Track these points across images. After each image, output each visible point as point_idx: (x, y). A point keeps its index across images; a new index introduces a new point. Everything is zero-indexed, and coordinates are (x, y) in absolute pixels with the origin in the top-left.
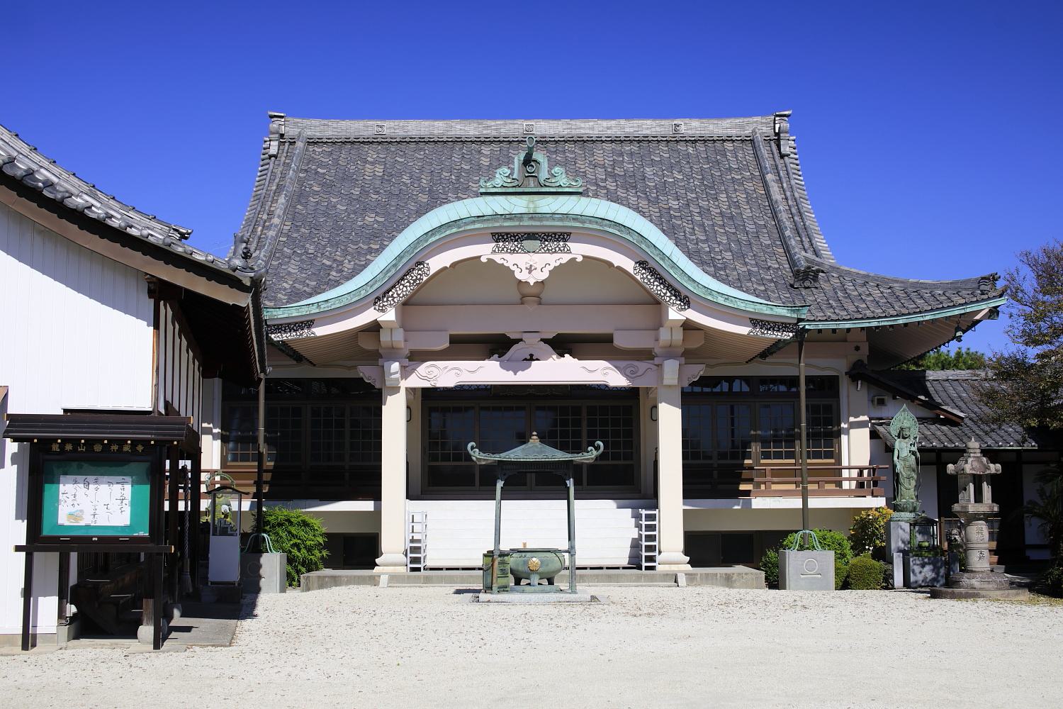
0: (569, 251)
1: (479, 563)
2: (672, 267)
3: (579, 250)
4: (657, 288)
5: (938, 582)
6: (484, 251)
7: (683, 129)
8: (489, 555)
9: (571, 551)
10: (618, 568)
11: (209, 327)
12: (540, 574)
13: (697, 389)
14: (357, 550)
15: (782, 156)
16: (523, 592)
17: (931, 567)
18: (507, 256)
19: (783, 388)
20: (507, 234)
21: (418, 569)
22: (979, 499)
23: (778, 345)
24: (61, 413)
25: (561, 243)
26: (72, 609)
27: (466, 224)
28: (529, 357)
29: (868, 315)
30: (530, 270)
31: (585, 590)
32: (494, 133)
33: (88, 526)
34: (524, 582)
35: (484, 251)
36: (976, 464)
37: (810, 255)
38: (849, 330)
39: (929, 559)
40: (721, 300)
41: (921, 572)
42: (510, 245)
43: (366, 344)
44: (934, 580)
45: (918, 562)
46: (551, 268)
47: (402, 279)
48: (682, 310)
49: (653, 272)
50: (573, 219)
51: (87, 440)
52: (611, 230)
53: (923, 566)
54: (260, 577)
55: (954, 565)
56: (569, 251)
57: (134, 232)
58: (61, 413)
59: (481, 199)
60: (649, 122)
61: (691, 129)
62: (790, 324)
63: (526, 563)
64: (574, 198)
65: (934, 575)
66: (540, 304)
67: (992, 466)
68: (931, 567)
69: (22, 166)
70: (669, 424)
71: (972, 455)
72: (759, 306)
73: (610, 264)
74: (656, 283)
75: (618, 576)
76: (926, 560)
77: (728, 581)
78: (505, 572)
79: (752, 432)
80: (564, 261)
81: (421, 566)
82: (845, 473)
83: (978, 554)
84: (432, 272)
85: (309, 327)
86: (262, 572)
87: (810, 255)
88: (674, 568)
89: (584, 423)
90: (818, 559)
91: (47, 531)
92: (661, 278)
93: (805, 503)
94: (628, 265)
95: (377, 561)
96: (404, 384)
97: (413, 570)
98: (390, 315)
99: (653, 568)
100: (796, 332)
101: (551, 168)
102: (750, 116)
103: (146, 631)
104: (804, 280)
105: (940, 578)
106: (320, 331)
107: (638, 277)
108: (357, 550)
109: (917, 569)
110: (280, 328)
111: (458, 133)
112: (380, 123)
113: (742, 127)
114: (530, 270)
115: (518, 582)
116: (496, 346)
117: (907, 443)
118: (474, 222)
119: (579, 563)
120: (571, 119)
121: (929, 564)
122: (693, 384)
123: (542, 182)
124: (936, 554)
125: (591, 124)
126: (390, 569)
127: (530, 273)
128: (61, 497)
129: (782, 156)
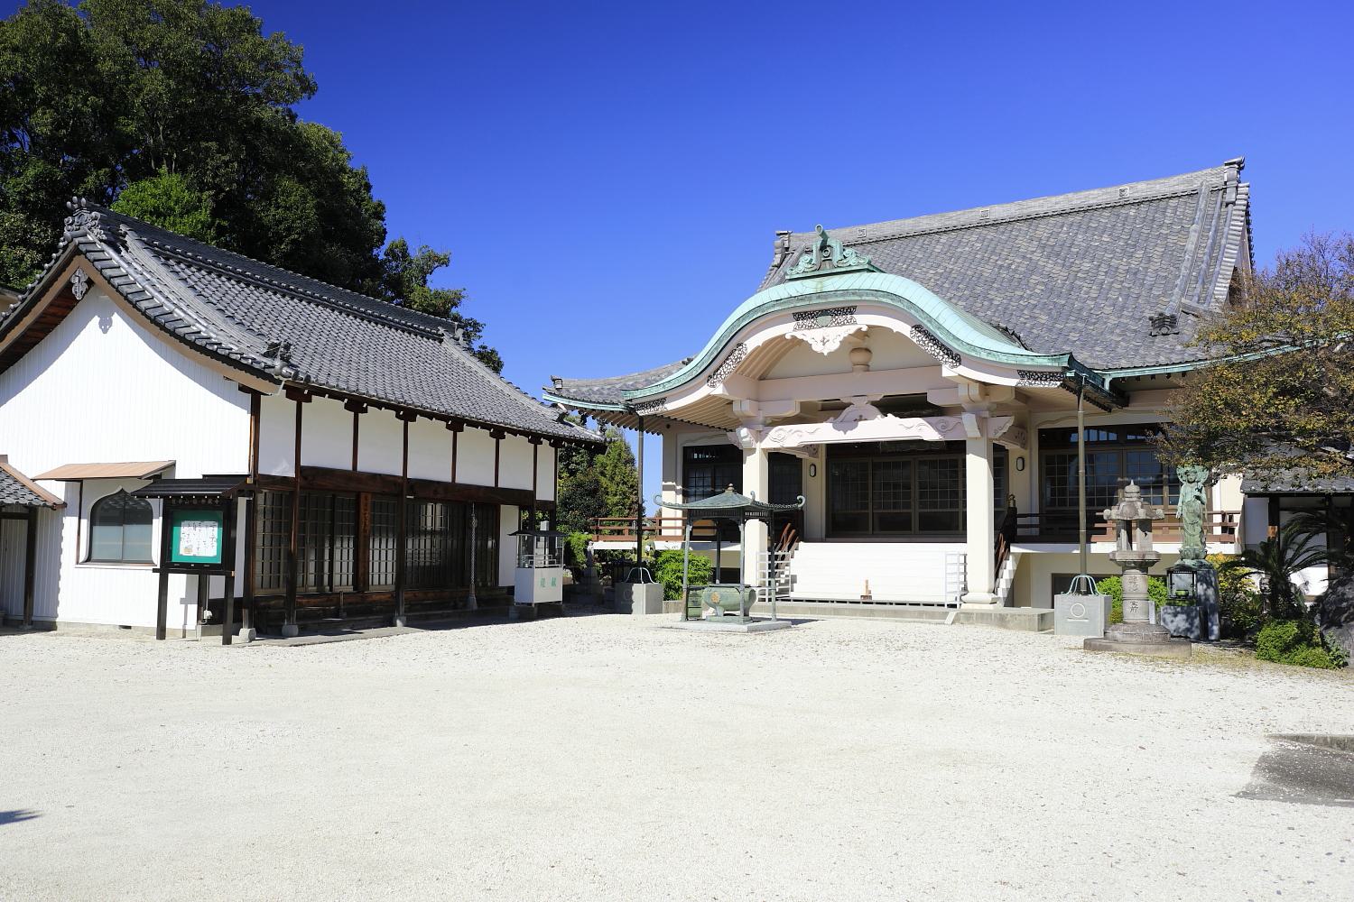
0: (855, 323)
2: (939, 328)
3: (863, 321)
4: (931, 348)
5: (1192, 632)
6: (788, 329)
7: (1128, 193)
10: (919, 605)
12: (722, 606)
17: (1184, 616)
18: (806, 332)
19: (1113, 437)
20: (805, 313)
24: (201, 477)
25: (849, 316)
26: (207, 614)
27: (768, 308)
28: (858, 418)
29: (1200, 357)
30: (824, 342)
33: (194, 556)
35: (788, 329)
36: (1127, 509)
39: (1182, 607)
40: (984, 355)
41: (1172, 621)
42: (808, 322)
44: (1188, 630)
45: (1169, 611)
46: (841, 338)
47: (727, 359)
48: (953, 367)
49: (927, 334)
50: (853, 294)
52: (884, 300)
53: (1175, 615)
54: (632, 602)
55: (1213, 615)
56: (855, 323)
58: (201, 477)
60: (1096, 192)
61: (1137, 192)
62: (1057, 373)
65: (1187, 625)
66: (868, 371)
68: (1184, 616)
70: (978, 472)
71: (1127, 499)
72: (1020, 358)
74: (930, 344)
75: (872, 611)
76: (1179, 609)
79: (1119, 479)
80: (851, 332)
83: (1131, 605)
84: (749, 351)
85: (663, 403)
86: (633, 597)
90: (1085, 603)
92: (935, 339)
94: (905, 329)
96: (759, 446)
100: (1063, 381)
102: (1200, 169)
104: (1160, 327)
105: (1194, 629)
106: (670, 406)
107: (915, 340)
109: (1169, 618)
110: (643, 406)
112: (861, 228)
113: (1190, 182)
114: (824, 342)
116: (831, 410)
117: (1192, 487)
120: (1024, 199)
121: (1182, 613)
123: (835, 264)
124: (1192, 604)
125: (1041, 201)
127: (824, 345)
128: (182, 536)
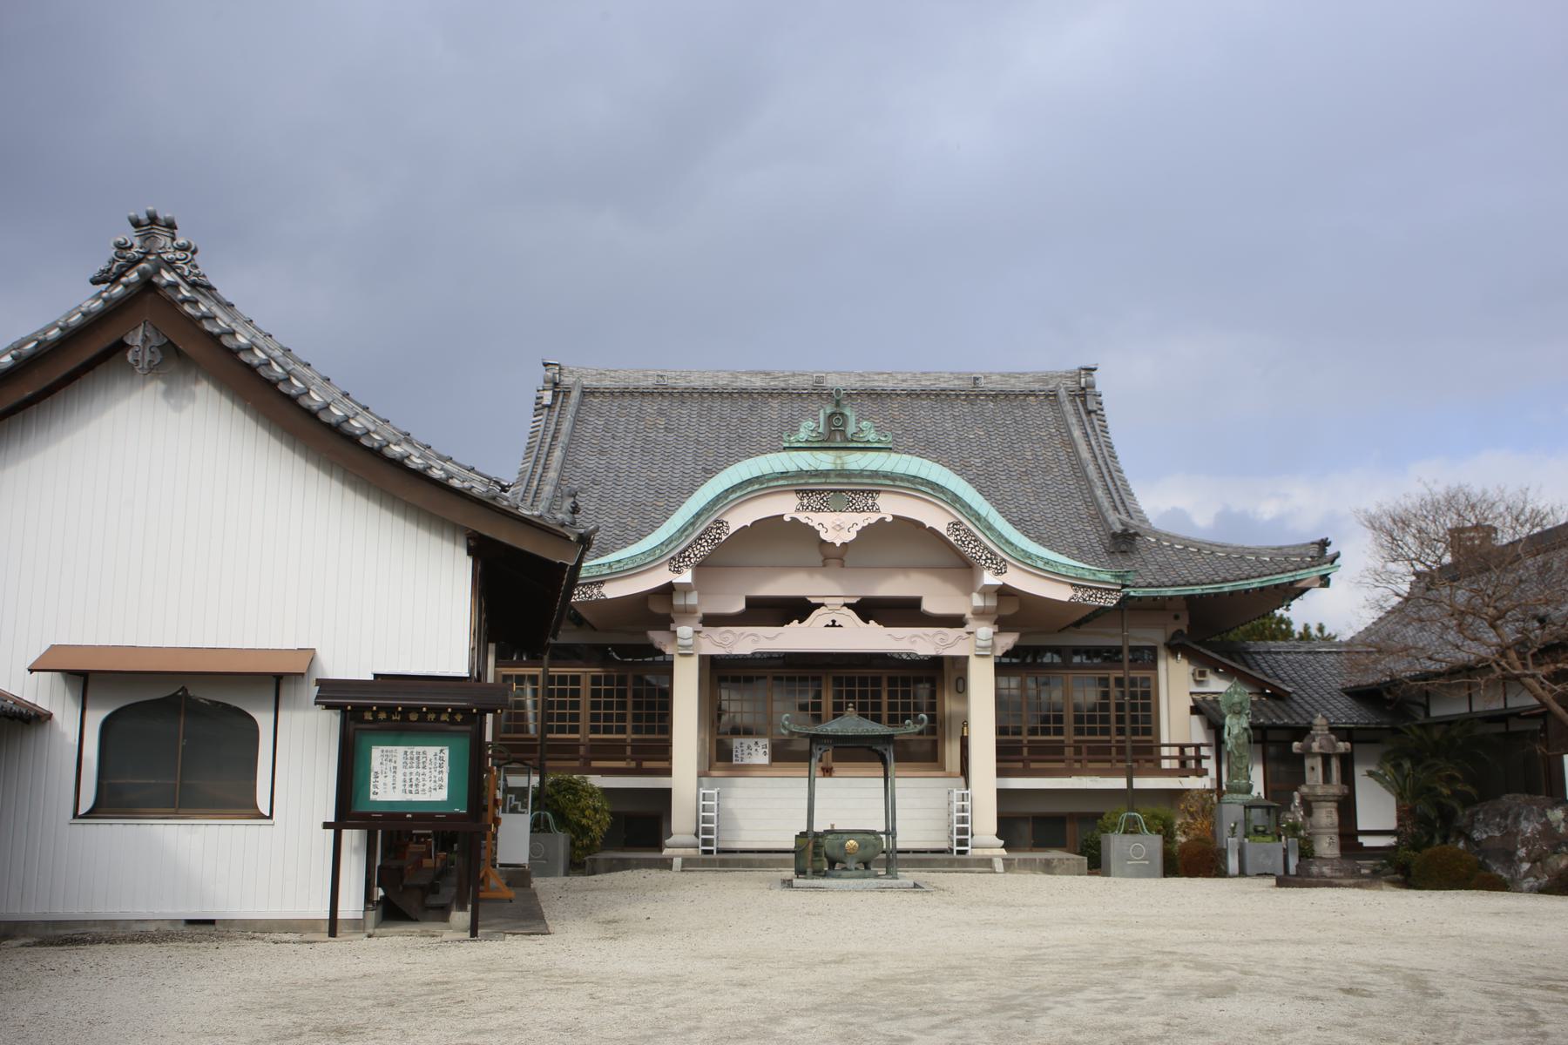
1: (792, 846)
3: (890, 506)
8: (803, 835)
9: (891, 832)
11: (521, 586)
13: (1006, 660)
14: (640, 829)
15: (1089, 413)
16: (839, 877)
18: (812, 515)
21: (711, 852)
22: (1327, 779)
23: (1102, 611)
27: (770, 480)
31: (908, 876)
32: (783, 385)
34: (838, 866)
35: (786, 506)
37: (1124, 517)
38: (1171, 598)
43: (657, 608)
51: (404, 707)
57: (456, 483)
59: (784, 455)
63: (842, 846)
64: (883, 454)
67: (1341, 744)
69: (337, 412)
73: (920, 525)
77: (1048, 868)
78: (818, 856)
80: (873, 521)
81: (714, 848)
82: (1165, 751)
87: (1124, 517)
88: (987, 852)
89: (630, 694)
91: (360, 808)
93: (1130, 783)
95: (668, 842)
97: (705, 852)
98: (686, 577)
99: (964, 852)
101: (858, 421)
103: (461, 918)
107: (952, 539)
108: (640, 829)
111: (744, 385)
115: (832, 864)
118: (777, 479)
119: (900, 846)
122: (1006, 654)
126: (681, 851)
129: (1089, 413)
